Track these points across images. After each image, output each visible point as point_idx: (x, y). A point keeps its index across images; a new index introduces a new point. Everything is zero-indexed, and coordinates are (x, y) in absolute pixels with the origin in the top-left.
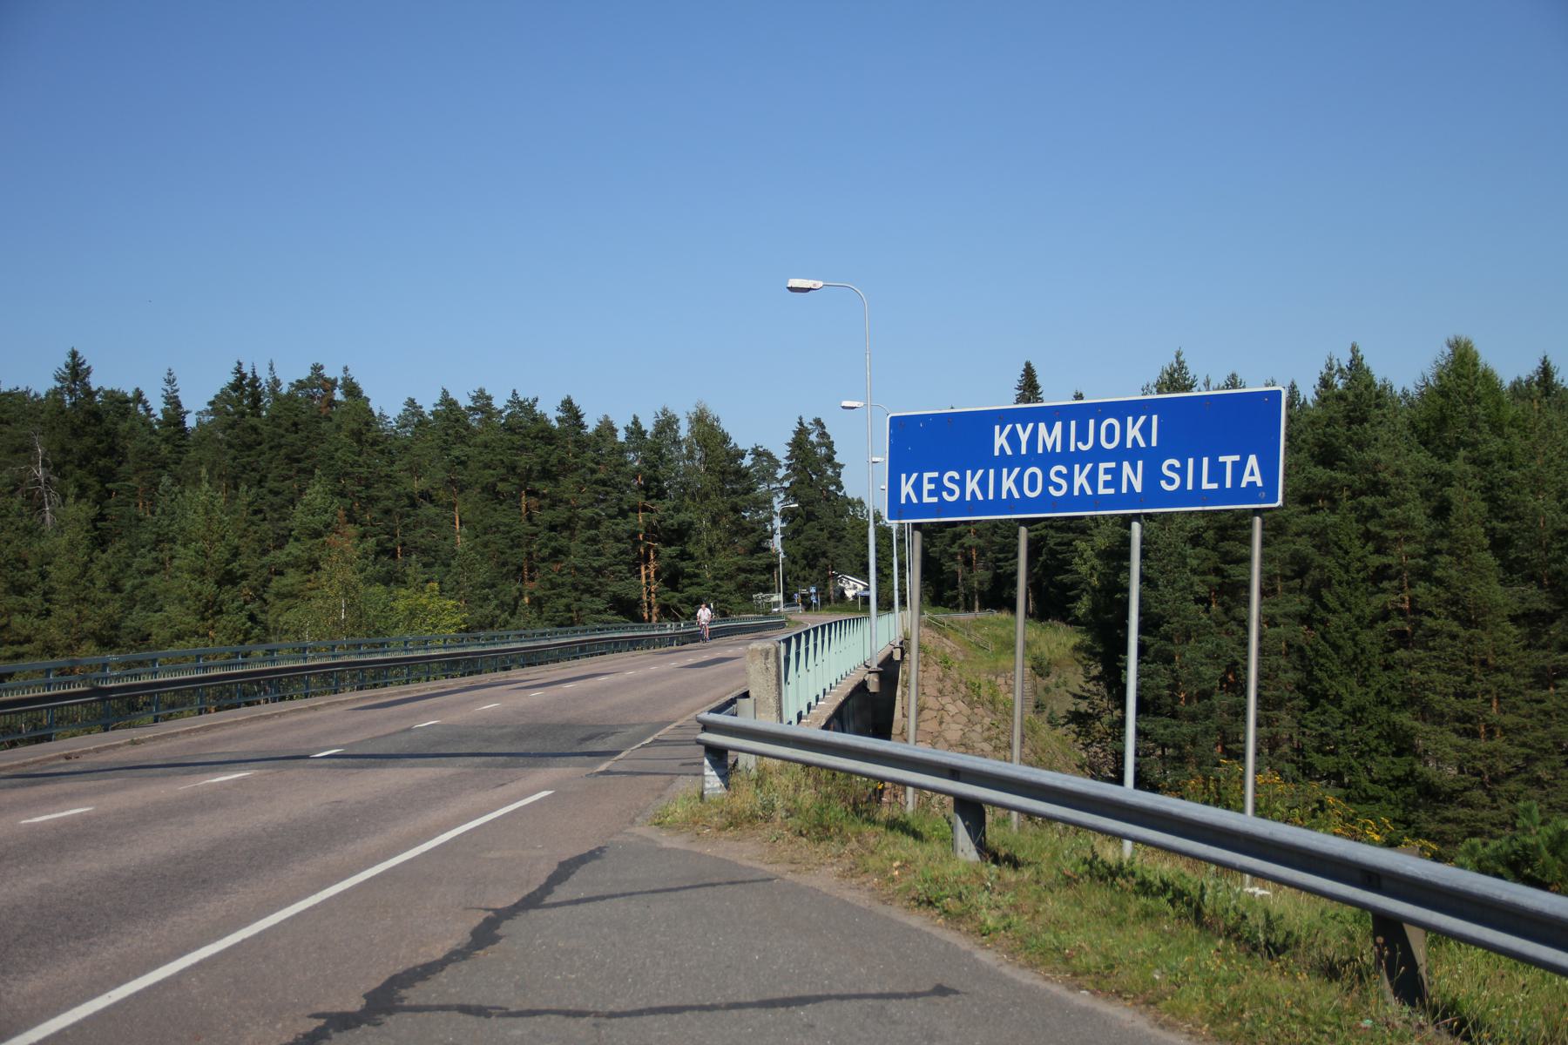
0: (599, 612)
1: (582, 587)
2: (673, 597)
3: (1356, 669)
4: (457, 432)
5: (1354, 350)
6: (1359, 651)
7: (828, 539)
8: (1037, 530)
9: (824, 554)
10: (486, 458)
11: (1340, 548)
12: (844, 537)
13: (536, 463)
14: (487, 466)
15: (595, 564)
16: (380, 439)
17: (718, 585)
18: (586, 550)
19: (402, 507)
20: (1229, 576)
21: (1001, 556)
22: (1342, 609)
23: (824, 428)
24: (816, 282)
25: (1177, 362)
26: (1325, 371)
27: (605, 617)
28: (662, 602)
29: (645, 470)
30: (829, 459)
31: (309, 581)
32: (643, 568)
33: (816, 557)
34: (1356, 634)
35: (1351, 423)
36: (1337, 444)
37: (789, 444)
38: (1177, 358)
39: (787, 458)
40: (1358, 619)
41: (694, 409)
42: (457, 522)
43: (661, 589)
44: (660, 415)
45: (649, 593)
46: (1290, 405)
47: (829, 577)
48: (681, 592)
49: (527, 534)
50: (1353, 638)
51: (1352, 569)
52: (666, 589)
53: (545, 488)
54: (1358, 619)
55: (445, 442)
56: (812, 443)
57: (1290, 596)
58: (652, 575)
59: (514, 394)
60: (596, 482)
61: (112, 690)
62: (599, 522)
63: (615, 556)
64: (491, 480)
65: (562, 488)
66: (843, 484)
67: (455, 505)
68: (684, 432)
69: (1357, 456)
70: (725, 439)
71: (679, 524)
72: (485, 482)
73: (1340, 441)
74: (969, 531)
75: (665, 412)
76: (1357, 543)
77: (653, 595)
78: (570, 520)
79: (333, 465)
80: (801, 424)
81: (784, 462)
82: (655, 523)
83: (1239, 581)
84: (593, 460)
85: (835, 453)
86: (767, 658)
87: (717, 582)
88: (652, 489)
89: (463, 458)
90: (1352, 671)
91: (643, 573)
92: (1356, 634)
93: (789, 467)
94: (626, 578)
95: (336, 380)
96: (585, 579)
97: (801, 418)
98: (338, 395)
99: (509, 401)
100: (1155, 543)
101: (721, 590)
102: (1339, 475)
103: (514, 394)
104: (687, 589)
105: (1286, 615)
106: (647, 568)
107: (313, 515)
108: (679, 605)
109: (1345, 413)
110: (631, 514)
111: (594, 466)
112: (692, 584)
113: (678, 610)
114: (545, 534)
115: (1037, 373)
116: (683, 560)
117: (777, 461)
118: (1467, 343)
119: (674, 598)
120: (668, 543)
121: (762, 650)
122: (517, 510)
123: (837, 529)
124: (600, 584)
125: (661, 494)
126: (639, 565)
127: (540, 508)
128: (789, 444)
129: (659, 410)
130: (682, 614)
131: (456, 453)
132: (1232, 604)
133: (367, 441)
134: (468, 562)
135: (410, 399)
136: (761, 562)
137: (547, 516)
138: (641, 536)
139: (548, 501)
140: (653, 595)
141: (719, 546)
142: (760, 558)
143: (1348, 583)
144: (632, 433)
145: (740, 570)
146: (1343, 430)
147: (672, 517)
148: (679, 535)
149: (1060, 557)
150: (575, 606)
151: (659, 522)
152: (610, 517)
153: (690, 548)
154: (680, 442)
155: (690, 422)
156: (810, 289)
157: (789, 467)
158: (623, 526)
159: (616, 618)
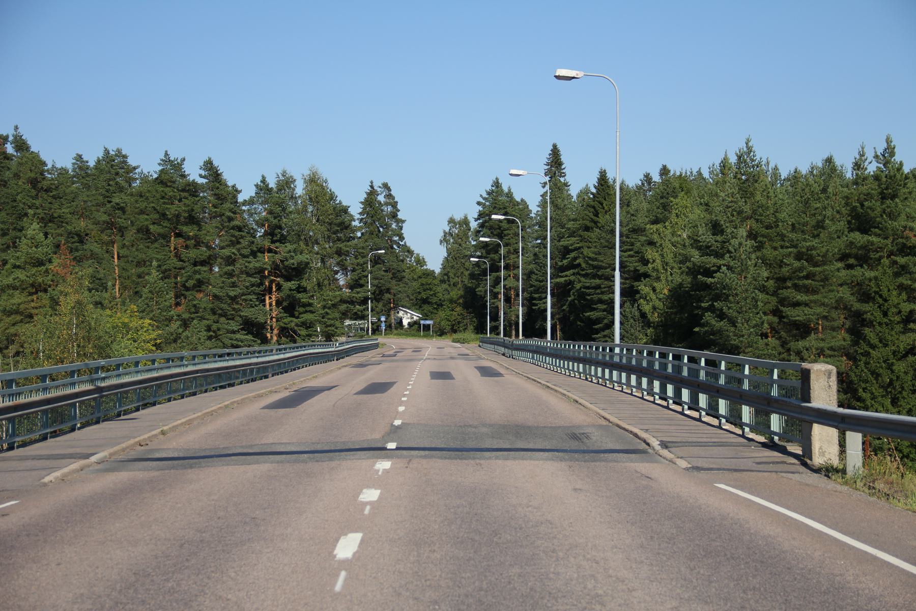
0: (234, 332)
1: (220, 312)
2: (292, 321)
3: (891, 392)
4: (117, 183)
5: (888, 141)
6: (895, 378)
7: (391, 279)
8: (566, 276)
9: (388, 291)
10: (142, 205)
11: (881, 296)
12: (404, 277)
13: (184, 211)
14: (142, 212)
15: (232, 294)
16: (53, 187)
17: (327, 313)
18: (223, 282)
19: (73, 243)
20: (787, 317)
21: (536, 296)
22: (880, 345)
23: (391, 190)
24: (578, 72)
25: (747, 147)
26: (858, 157)
27: (238, 336)
28: (283, 325)
29: (272, 220)
30: (394, 216)
31: (33, 301)
32: (267, 298)
33: (381, 292)
34: (892, 364)
35: (883, 198)
36: (873, 215)
37: (361, 203)
38: (747, 144)
39: (360, 214)
40: (894, 353)
41: (308, 172)
42: (116, 257)
43: (282, 315)
44: (280, 175)
45: (271, 319)
46: (621, 189)
47: (391, 308)
48: (297, 318)
49: (175, 268)
50: (890, 367)
51: (890, 314)
52: (286, 315)
53: (191, 231)
54: (894, 353)
55: (107, 191)
56: (380, 203)
57: (835, 334)
58: (274, 304)
59: (166, 154)
60: (233, 228)
61: (109, 388)
62: (234, 260)
63: (247, 287)
64: (146, 223)
65: (204, 232)
66: (404, 235)
67: (114, 243)
68: (300, 189)
69: (891, 224)
70: (332, 197)
71: (298, 263)
72: (141, 224)
73: (876, 212)
74: (510, 276)
75: (284, 174)
76: (895, 293)
77: (274, 320)
78: (210, 257)
79: (15, 207)
80: (372, 187)
81: (357, 216)
82: (278, 262)
83: (796, 321)
84: (231, 211)
85: (399, 211)
86: (829, 377)
87: (326, 310)
88: (276, 235)
89: (122, 205)
90: (887, 393)
91: (267, 301)
92: (892, 364)
93: (361, 220)
94: (256, 305)
95: (7, 137)
96: (223, 305)
97: (372, 182)
98: (10, 149)
99: (162, 160)
100: (735, 289)
101: (329, 317)
102: (874, 239)
103: (166, 154)
104: (302, 315)
105: (831, 349)
106: (270, 298)
107: (36, 247)
108: (296, 328)
109: (879, 190)
110: (259, 254)
111: (232, 215)
112: (306, 312)
113: (295, 332)
114: (190, 269)
115: (561, 153)
116: (299, 292)
117: (352, 216)
118: (119, 152)
119: (292, 322)
120: (288, 279)
121: (826, 371)
122: (167, 248)
123: (399, 271)
124: (234, 309)
125: (283, 240)
126: (264, 295)
127: (187, 247)
128: (361, 203)
129: (280, 172)
130: (299, 336)
131: (116, 200)
132: (788, 339)
133: (42, 188)
134: (157, 289)
135: (78, 155)
136: (360, 295)
137: (193, 254)
138: (266, 272)
139: (193, 241)
140: (274, 320)
141: (326, 282)
142: (358, 293)
143: (887, 325)
144: (261, 190)
145: (343, 301)
146: (878, 203)
147: (292, 257)
148: (297, 272)
149: (589, 298)
150: (214, 327)
151: (282, 261)
152: (244, 256)
153: (304, 283)
154: (296, 198)
155: (305, 182)
156: (574, 78)
157: (361, 220)
158: (254, 264)
159: (246, 337)
